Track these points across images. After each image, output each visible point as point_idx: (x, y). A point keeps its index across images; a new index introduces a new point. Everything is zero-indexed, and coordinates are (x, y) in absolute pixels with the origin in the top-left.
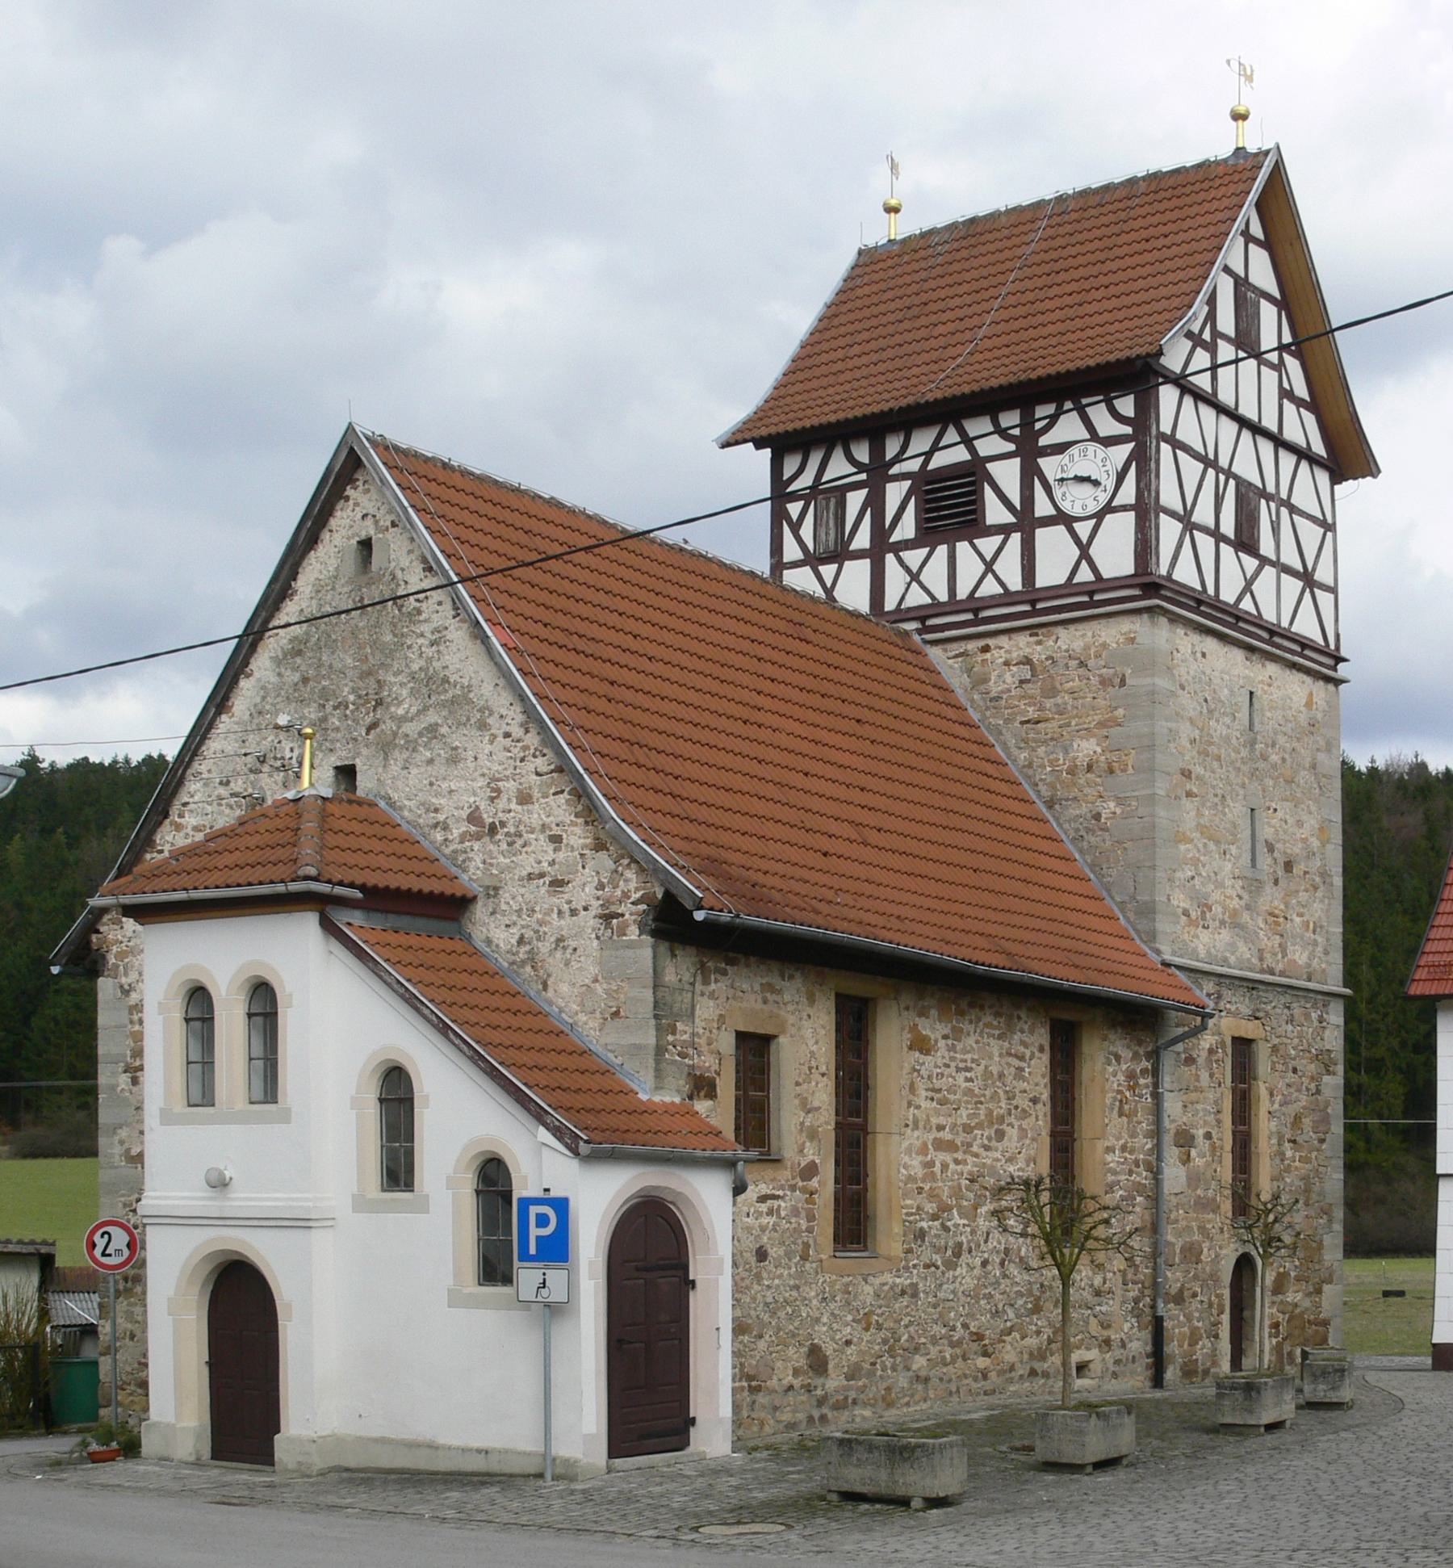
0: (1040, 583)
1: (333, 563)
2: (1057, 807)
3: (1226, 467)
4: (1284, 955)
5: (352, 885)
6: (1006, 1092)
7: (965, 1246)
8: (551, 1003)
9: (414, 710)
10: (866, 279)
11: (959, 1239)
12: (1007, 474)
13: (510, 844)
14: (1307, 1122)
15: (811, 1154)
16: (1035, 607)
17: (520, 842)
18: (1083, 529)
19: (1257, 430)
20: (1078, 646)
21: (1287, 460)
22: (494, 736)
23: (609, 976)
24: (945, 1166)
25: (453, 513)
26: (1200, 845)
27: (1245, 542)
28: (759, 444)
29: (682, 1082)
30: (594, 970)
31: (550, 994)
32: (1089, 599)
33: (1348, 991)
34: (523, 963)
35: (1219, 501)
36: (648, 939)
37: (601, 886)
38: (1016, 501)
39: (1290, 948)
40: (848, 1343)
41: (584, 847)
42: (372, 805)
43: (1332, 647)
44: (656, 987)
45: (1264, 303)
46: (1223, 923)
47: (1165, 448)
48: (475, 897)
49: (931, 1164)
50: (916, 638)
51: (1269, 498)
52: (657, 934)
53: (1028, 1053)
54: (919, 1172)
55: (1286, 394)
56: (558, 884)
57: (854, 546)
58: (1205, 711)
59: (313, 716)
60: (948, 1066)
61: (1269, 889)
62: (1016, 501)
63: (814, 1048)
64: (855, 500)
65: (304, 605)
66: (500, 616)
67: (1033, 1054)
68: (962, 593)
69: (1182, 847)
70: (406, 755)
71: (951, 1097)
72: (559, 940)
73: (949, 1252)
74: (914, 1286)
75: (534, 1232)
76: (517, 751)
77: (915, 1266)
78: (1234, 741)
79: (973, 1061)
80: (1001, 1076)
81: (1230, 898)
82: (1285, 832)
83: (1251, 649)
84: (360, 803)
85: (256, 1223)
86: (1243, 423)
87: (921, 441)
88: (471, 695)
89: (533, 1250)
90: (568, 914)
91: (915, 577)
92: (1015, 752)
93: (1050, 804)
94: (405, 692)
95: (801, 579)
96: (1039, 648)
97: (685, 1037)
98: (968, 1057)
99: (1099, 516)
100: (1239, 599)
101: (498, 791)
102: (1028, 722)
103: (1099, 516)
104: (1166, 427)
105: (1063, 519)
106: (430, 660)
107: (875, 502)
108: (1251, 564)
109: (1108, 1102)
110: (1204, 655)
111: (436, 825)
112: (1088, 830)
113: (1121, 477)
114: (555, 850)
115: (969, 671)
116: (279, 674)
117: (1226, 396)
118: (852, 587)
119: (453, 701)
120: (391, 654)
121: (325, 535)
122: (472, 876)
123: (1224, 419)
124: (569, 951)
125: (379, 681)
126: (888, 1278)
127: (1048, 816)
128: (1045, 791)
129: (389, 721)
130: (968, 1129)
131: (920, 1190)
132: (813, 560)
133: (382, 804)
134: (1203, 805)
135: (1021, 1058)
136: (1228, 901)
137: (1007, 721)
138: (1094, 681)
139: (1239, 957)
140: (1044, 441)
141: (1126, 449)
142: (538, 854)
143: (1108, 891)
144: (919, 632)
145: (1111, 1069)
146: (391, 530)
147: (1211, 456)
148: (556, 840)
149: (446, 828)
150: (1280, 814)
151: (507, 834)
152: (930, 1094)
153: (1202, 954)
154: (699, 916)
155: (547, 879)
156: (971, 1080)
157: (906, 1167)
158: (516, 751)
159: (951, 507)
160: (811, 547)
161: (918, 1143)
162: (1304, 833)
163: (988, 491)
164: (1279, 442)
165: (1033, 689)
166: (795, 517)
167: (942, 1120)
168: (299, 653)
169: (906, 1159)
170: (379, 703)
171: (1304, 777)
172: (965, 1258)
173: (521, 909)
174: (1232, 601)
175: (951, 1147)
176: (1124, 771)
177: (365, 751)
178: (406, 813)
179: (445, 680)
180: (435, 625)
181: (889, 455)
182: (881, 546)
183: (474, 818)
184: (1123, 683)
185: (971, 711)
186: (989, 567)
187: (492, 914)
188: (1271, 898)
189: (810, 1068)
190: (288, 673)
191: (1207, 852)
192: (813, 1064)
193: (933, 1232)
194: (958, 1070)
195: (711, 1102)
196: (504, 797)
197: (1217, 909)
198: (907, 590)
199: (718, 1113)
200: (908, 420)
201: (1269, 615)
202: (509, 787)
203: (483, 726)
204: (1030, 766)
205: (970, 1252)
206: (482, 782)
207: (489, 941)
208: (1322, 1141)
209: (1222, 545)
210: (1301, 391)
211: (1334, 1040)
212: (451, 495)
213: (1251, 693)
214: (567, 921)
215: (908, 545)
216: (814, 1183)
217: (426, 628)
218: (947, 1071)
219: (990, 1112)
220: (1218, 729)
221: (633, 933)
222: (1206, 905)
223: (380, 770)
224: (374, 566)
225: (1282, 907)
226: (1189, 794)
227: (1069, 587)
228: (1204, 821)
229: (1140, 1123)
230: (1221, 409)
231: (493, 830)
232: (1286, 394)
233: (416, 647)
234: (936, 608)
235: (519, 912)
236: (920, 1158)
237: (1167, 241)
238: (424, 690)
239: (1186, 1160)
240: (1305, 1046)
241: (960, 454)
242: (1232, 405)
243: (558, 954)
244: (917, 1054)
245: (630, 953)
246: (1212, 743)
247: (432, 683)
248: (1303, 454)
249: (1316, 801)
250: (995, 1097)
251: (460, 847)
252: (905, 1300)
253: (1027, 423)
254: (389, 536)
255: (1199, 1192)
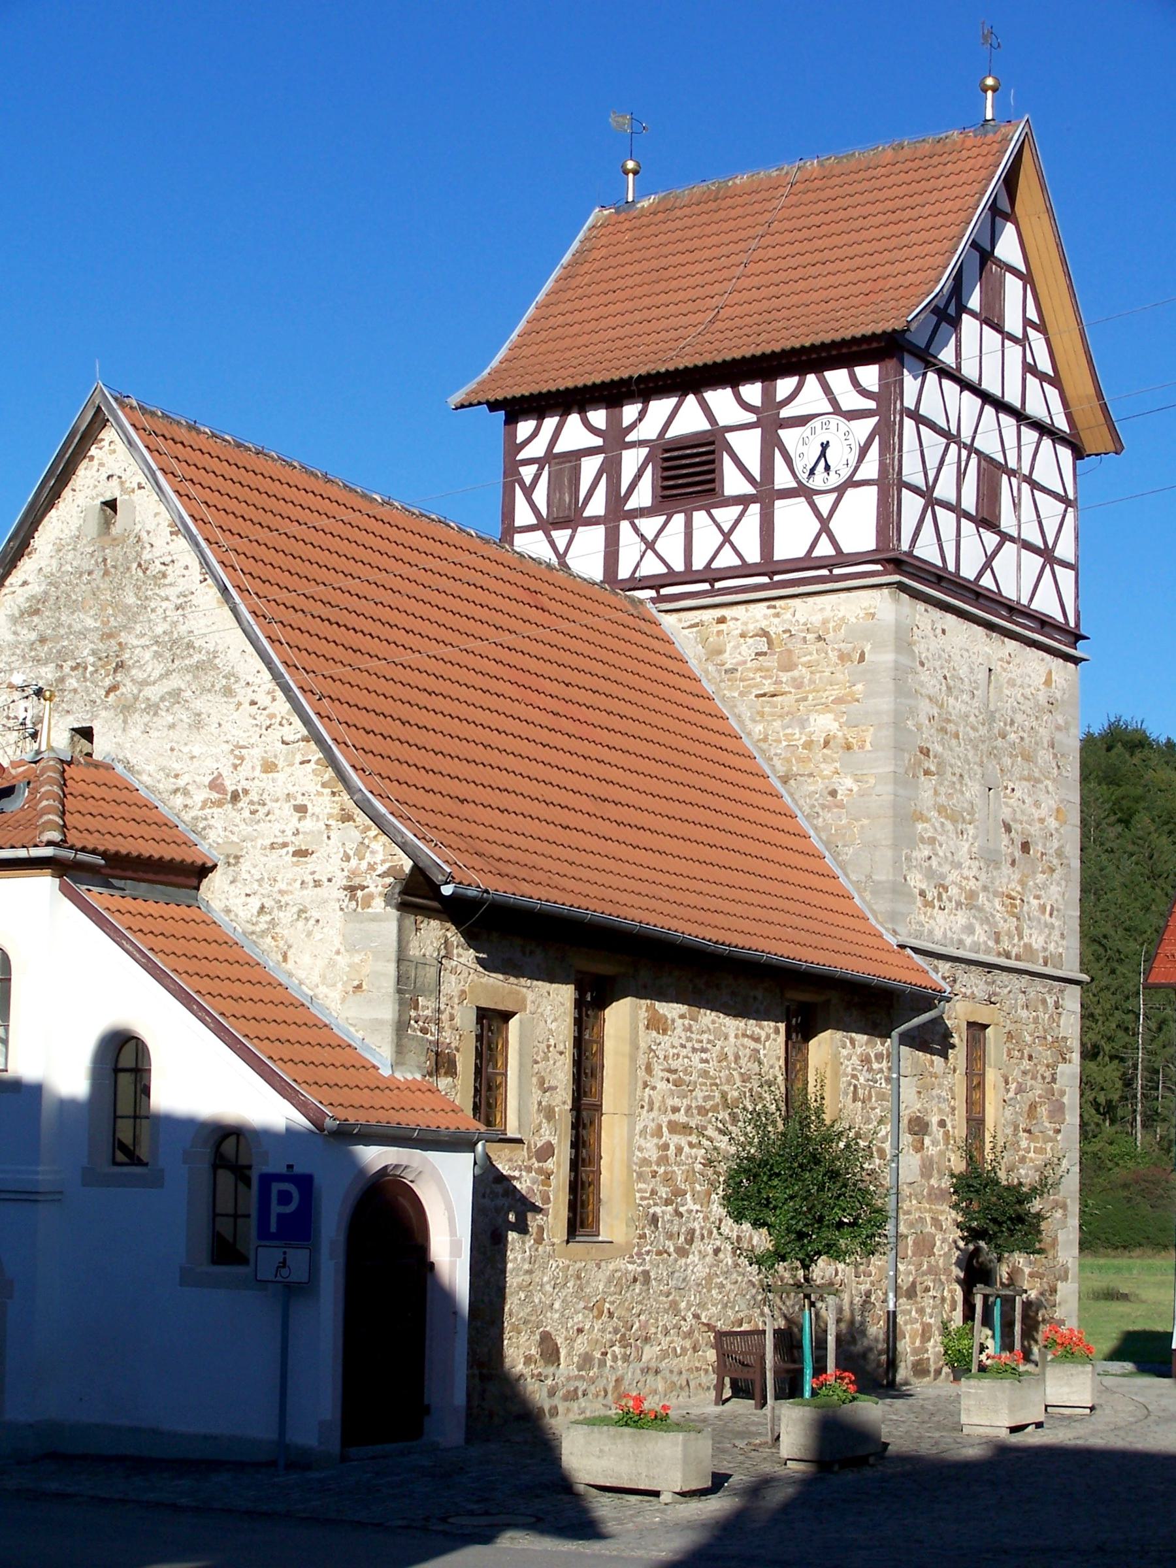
0: (778, 555)
1: (75, 523)
2: (792, 782)
3: (968, 442)
4: (1021, 938)
5: (94, 852)
6: (741, 1074)
7: (698, 1233)
8: (291, 975)
9: (156, 674)
10: (604, 241)
11: (690, 1225)
12: (747, 445)
13: (253, 813)
14: (1043, 1111)
15: (547, 1135)
16: (774, 576)
17: (262, 811)
18: (824, 503)
19: (1001, 406)
20: (816, 619)
21: (1030, 435)
22: (239, 704)
23: (352, 949)
24: (679, 1150)
25: (199, 475)
26: (937, 825)
27: (987, 520)
28: (494, 406)
29: (423, 1059)
30: (337, 942)
31: (290, 966)
32: (824, 571)
33: (1085, 978)
34: (263, 933)
35: (961, 476)
36: (393, 913)
37: (347, 858)
38: (756, 473)
39: (1026, 932)
40: (580, 1331)
41: (330, 816)
42: (110, 768)
43: (1072, 624)
44: (399, 961)
45: (1009, 277)
46: (959, 904)
47: (909, 423)
48: (215, 866)
49: (666, 1147)
50: (650, 605)
51: (1012, 473)
52: (403, 907)
53: (763, 1035)
54: (654, 1155)
55: (1030, 369)
56: (301, 853)
57: (588, 512)
58: (944, 688)
59: (50, 676)
60: (683, 1046)
61: (1006, 869)
62: (756, 473)
63: (553, 1026)
64: (590, 467)
65: (43, 565)
66: (246, 582)
67: (768, 1037)
68: (698, 564)
69: (920, 826)
70: (146, 718)
71: (687, 1078)
72: (301, 911)
73: (682, 1239)
74: (646, 1273)
75: (276, 1209)
76: (262, 719)
77: (648, 1252)
78: (972, 719)
79: (709, 1041)
80: (737, 1058)
81: (967, 879)
82: (1023, 812)
83: (990, 626)
84: (97, 765)
85: (13, 1196)
86: (986, 398)
87: (660, 408)
88: (217, 661)
89: (273, 1228)
90: (312, 884)
91: (650, 545)
92: (750, 725)
93: (785, 780)
94: (148, 655)
95: (533, 545)
96: (776, 621)
97: (427, 1013)
98: (705, 1037)
99: (841, 490)
100: (980, 575)
101: (242, 758)
102: (764, 695)
103: (841, 490)
104: (909, 402)
105: (802, 491)
106: (174, 624)
107: (611, 469)
108: (991, 539)
109: (842, 1086)
110: (944, 632)
111: (176, 791)
112: (823, 807)
113: (864, 451)
114: (300, 820)
115: (705, 641)
116: (15, 633)
117: (969, 371)
118: (586, 553)
119: (199, 667)
120: (133, 618)
121: (67, 493)
122: (209, 846)
123: (966, 393)
124: (312, 922)
125: (120, 644)
126: (621, 1264)
127: (782, 790)
128: (781, 769)
129: (129, 684)
130: (702, 1111)
131: (654, 1174)
132: (546, 525)
133: (119, 768)
134: (941, 784)
135: (757, 1040)
136: (964, 883)
137: (742, 694)
138: (834, 656)
139: (976, 941)
140: (785, 413)
141: (871, 423)
142: (284, 821)
143: (843, 869)
144: (653, 600)
145: (844, 1052)
146: (138, 492)
147: (954, 432)
148: (301, 809)
149: (186, 793)
150: (1018, 794)
151: (252, 803)
152: (667, 1075)
153: (938, 934)
154: (447, 890)
155: (291, 849)
156: (707, 1061)
157: (640, 1149)
158: (262, 718)
159: (688, 474)
160: (544, 512)
161: (652, 1125)
162: (1043, 812)
163: (727, 460)
164: (1020, 416)
165: (770, 662)
166: (528, 481)
167: (677, 1102)
168: (37, 612)
169: (642, 1142)
170: (120, 666)
171: (1044, 756)
172: (697, 1244)
173: (262, 879)
174: (971, 576)
175: (686, 1129)
176: (862, 747)
177: (104, 713)
178: (145, 778)
179: (190, 645)
180: (180, 589)
181: (626, 422)
182: (618, 511)
183: (216, 785)
184: (862, 658)
185: (704, 682)
186: (727, 537)
187: (232, 882)
188: (1008, 879)
189: (549, 1047)
190: (25, 631)
191: (945, 832)
192: (552, 1042)
193: (667, 1217)
194: (694, 1050)
195: (450, 1079)
196: (247, 765)
197: (953, 891)
198: (642, 557)
199: (458, 1090)
200: (648, 387)
201: (1009, 592)
202: (254, 756)
203: (228, 692)
204: (765, 740)
205: (703, 1238)
206: (227, 748)
207: (228, 911)
208: (1058, 1131)
209: (963, 520)
210: (1045, 365)
211: (1070, 1027)
212: (196, 457)
213: (990, 670)
214: (310, 892)
215: (642, 512)
216: (550, 1164)
217: (171, 592)
218: (684, 1052)
219: (724, 1095)
220: (956, 706)
221: (378, 904)
222: (942, 886)
223: (119, 732)
224: (115, 530)
225: (1019, 889)
226: (927, 773)
227: (807, 562)
228: (942, 799)
229: (873, 1109)
230: (965, 385)
231: (235, 797)
232: (1030, 369)
233: (160, 611)
234: (672, 578)
235: (260, 881)
236: (655, 1140)
237: (914, 214)
238: (168, 654)
239: (919, 1148)
240: (1042, 1034)
241: (700, 424)
242: (975, 379)
243: (300, 924)
244: (654, 1034)
245: (374, 926)
246: (948, 721)
247: (175, 647)
248: (1044, 429)
249: (1054, 780)
250: (730, 1080)
251: (200, 813)
252: (638, 1287)
253: (768, 395)
254: (134, 497)
255: (933, 1182)
